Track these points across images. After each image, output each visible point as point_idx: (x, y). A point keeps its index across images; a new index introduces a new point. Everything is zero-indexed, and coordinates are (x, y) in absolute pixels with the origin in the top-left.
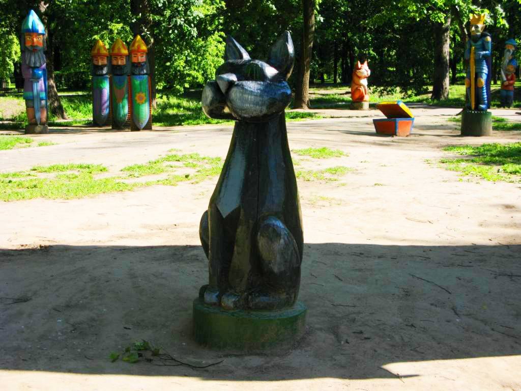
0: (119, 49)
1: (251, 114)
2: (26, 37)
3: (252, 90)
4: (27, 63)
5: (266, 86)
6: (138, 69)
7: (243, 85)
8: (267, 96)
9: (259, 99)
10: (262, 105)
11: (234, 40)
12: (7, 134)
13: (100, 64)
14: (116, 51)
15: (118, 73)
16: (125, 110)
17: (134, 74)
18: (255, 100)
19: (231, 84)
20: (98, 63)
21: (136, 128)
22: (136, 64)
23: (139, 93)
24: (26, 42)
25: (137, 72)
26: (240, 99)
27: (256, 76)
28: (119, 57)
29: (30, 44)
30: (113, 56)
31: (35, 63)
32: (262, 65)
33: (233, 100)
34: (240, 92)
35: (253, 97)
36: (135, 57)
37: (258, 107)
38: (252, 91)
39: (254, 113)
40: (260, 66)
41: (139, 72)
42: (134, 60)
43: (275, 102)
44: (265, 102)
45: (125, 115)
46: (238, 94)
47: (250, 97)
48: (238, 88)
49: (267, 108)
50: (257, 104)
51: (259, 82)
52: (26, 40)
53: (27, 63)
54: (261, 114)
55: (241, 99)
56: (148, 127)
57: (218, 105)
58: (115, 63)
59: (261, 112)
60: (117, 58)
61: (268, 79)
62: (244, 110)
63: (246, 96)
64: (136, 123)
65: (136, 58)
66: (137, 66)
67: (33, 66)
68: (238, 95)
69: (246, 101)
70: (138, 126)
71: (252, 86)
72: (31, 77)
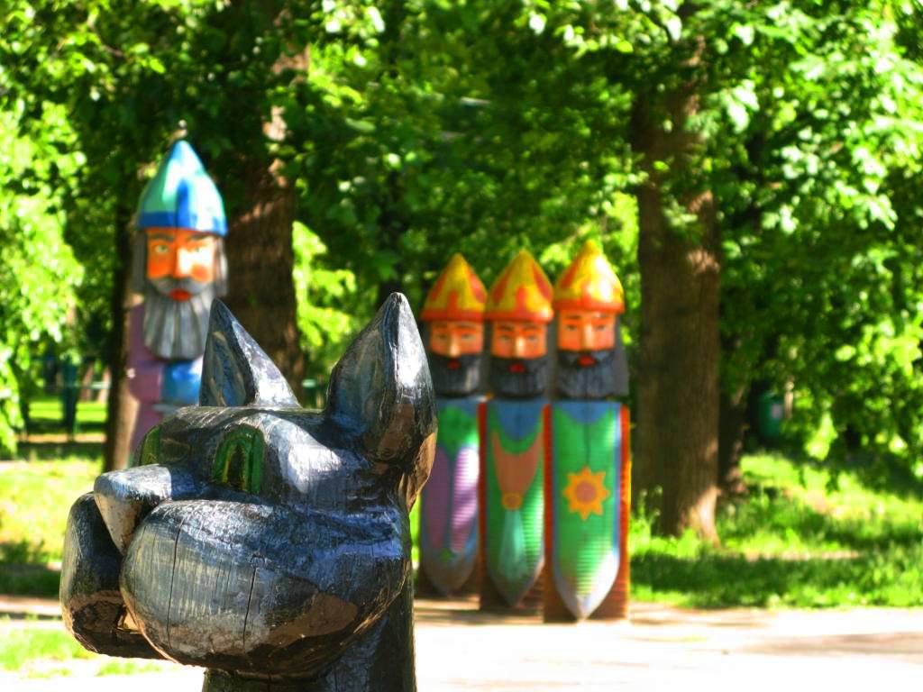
0: (521, 294)
1: (205, 644)
2: (151, 244)
3: (210, 539)
4: (149, 341)
5: (273, 526)
6: (580, 377)
7: (178, 520)
8: (270, 568)
9: (234, 579)
10: (248, 607)
11: (235, 323)
12: (42, 617)
13: (455, 350)
14: (509, 303)
15: (513, 386)
16: (528, 533)
17: (562, 396)
18: (218, 585)
19: (143, 510)
20: (448, 346)
21: (562, 613)
22: (572, 359)
23: (579, 471)
24: (152, 261)
25: (575, 390)
26: (164, 580)
27: (250, 479)
28: (518, 328)
29: (165, 271)
30: (496, 325)
31: (177, 344)
32: (275, 435)
33: (137, 580)
34: (165, 549)
35: (211, 572)
36: (572, 327)
37: (230, 615)
38: (209, 547)
39: (218, 639)
40: (267, 439)
41: (584, 387)
42: (568, 339)
43: (307, 596)
44: (260, 595)
45: (529, 558)
46: (156, 556)
47: (200, 569)
48: (158, 532)
49: (268, 622)
50: (225, 601)
51: (254, 508)
52: (151, 256)
53: (149, 341)
54: (246, 647)
55: (170, 577)
56: (610, 609)
57: (95, 597)
58: (500, 347)
59: (245, 634)
60: (509, 329)
61: (298, 493)
62: (175, 625)
63: (186, 565)
64: (564, 595)
65: (575, 332)
66: (578, 365)
67: (166, 351)
68: (160, 559)
69: (187, 589)
70: (569, 604)
71: (216, 520)
72: (159, 396)
